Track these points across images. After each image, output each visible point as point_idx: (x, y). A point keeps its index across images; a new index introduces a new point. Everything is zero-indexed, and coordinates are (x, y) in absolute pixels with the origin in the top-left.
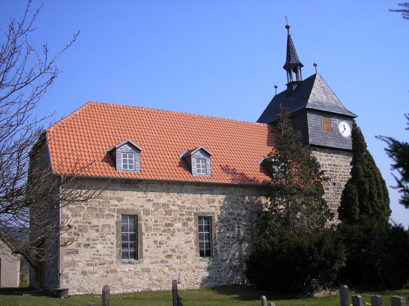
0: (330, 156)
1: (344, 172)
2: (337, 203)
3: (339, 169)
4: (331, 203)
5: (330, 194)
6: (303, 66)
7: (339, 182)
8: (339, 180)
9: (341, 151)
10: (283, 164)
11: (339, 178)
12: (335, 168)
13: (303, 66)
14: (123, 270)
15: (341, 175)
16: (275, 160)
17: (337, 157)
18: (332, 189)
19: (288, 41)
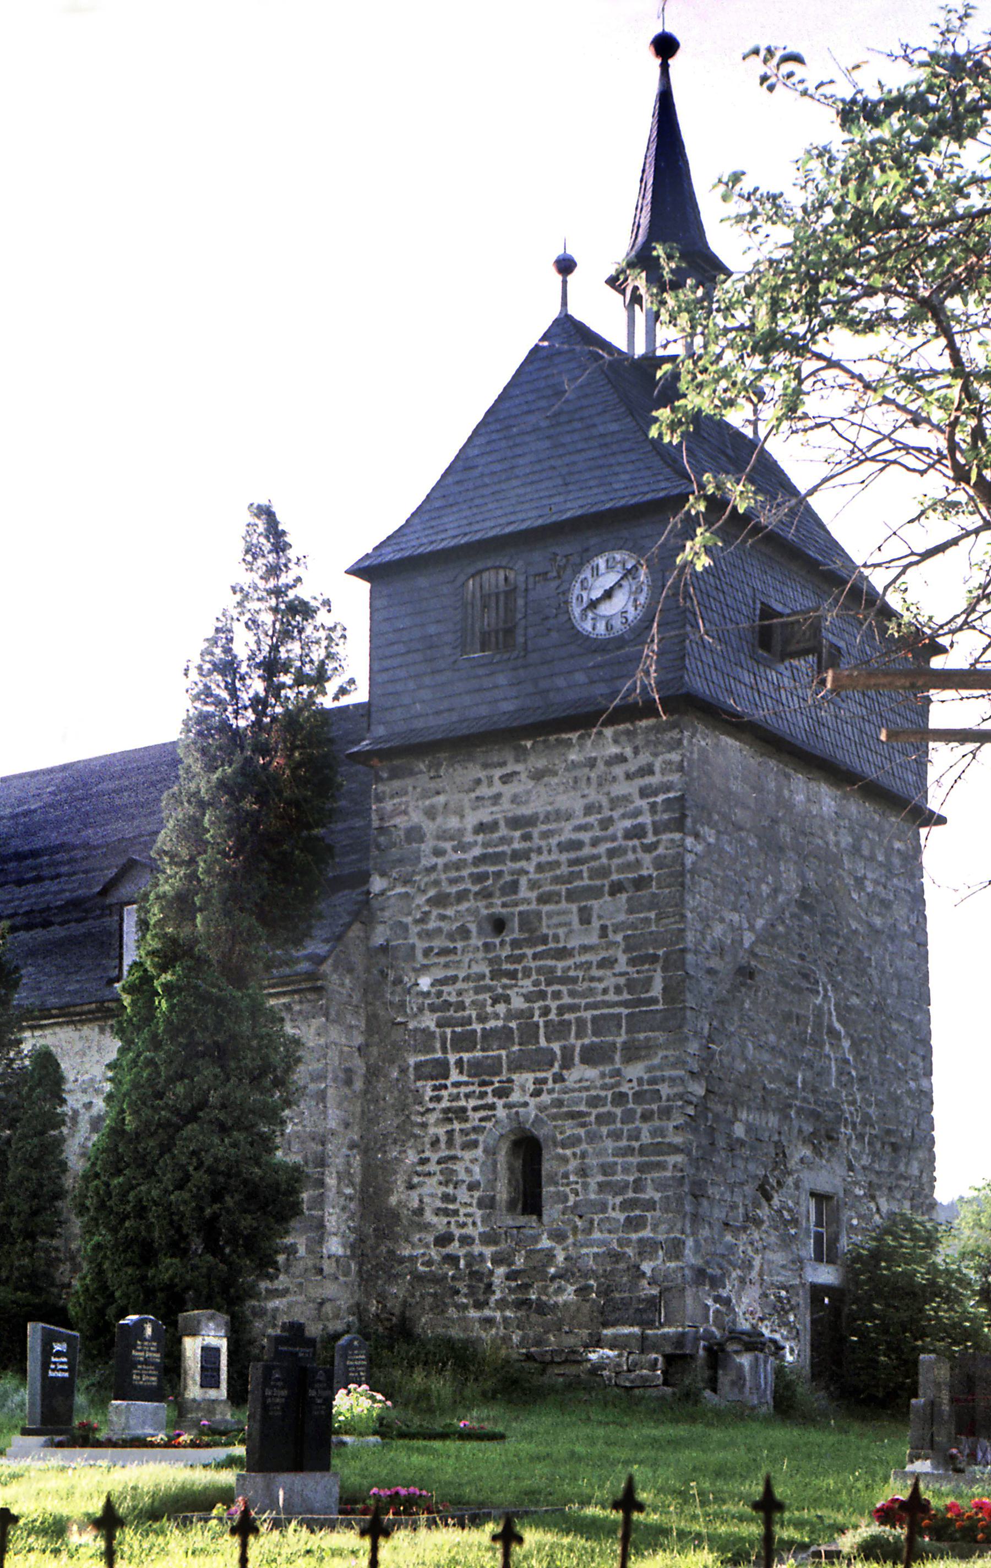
0: (496, 779)
1: (578, 845)
2: (500, 1023)
3: (545, 835)
4: (459, 1029)
5: (460, 985)
6: (347, 572)
7: (534, 906)
8: (533, 895)
9: (573, 729)
10: (473, 1313)
11: (533, 885)
12: (517, 834)
13: (347, 572)
14: (806, 386)
15: (458, 865)
16: (683, 840)
17: (538, 776)
18: (480, 955)
19: (131, 1447)
